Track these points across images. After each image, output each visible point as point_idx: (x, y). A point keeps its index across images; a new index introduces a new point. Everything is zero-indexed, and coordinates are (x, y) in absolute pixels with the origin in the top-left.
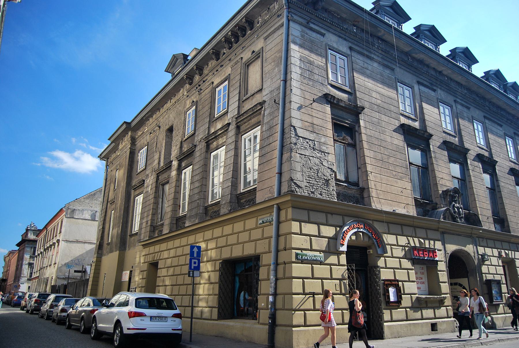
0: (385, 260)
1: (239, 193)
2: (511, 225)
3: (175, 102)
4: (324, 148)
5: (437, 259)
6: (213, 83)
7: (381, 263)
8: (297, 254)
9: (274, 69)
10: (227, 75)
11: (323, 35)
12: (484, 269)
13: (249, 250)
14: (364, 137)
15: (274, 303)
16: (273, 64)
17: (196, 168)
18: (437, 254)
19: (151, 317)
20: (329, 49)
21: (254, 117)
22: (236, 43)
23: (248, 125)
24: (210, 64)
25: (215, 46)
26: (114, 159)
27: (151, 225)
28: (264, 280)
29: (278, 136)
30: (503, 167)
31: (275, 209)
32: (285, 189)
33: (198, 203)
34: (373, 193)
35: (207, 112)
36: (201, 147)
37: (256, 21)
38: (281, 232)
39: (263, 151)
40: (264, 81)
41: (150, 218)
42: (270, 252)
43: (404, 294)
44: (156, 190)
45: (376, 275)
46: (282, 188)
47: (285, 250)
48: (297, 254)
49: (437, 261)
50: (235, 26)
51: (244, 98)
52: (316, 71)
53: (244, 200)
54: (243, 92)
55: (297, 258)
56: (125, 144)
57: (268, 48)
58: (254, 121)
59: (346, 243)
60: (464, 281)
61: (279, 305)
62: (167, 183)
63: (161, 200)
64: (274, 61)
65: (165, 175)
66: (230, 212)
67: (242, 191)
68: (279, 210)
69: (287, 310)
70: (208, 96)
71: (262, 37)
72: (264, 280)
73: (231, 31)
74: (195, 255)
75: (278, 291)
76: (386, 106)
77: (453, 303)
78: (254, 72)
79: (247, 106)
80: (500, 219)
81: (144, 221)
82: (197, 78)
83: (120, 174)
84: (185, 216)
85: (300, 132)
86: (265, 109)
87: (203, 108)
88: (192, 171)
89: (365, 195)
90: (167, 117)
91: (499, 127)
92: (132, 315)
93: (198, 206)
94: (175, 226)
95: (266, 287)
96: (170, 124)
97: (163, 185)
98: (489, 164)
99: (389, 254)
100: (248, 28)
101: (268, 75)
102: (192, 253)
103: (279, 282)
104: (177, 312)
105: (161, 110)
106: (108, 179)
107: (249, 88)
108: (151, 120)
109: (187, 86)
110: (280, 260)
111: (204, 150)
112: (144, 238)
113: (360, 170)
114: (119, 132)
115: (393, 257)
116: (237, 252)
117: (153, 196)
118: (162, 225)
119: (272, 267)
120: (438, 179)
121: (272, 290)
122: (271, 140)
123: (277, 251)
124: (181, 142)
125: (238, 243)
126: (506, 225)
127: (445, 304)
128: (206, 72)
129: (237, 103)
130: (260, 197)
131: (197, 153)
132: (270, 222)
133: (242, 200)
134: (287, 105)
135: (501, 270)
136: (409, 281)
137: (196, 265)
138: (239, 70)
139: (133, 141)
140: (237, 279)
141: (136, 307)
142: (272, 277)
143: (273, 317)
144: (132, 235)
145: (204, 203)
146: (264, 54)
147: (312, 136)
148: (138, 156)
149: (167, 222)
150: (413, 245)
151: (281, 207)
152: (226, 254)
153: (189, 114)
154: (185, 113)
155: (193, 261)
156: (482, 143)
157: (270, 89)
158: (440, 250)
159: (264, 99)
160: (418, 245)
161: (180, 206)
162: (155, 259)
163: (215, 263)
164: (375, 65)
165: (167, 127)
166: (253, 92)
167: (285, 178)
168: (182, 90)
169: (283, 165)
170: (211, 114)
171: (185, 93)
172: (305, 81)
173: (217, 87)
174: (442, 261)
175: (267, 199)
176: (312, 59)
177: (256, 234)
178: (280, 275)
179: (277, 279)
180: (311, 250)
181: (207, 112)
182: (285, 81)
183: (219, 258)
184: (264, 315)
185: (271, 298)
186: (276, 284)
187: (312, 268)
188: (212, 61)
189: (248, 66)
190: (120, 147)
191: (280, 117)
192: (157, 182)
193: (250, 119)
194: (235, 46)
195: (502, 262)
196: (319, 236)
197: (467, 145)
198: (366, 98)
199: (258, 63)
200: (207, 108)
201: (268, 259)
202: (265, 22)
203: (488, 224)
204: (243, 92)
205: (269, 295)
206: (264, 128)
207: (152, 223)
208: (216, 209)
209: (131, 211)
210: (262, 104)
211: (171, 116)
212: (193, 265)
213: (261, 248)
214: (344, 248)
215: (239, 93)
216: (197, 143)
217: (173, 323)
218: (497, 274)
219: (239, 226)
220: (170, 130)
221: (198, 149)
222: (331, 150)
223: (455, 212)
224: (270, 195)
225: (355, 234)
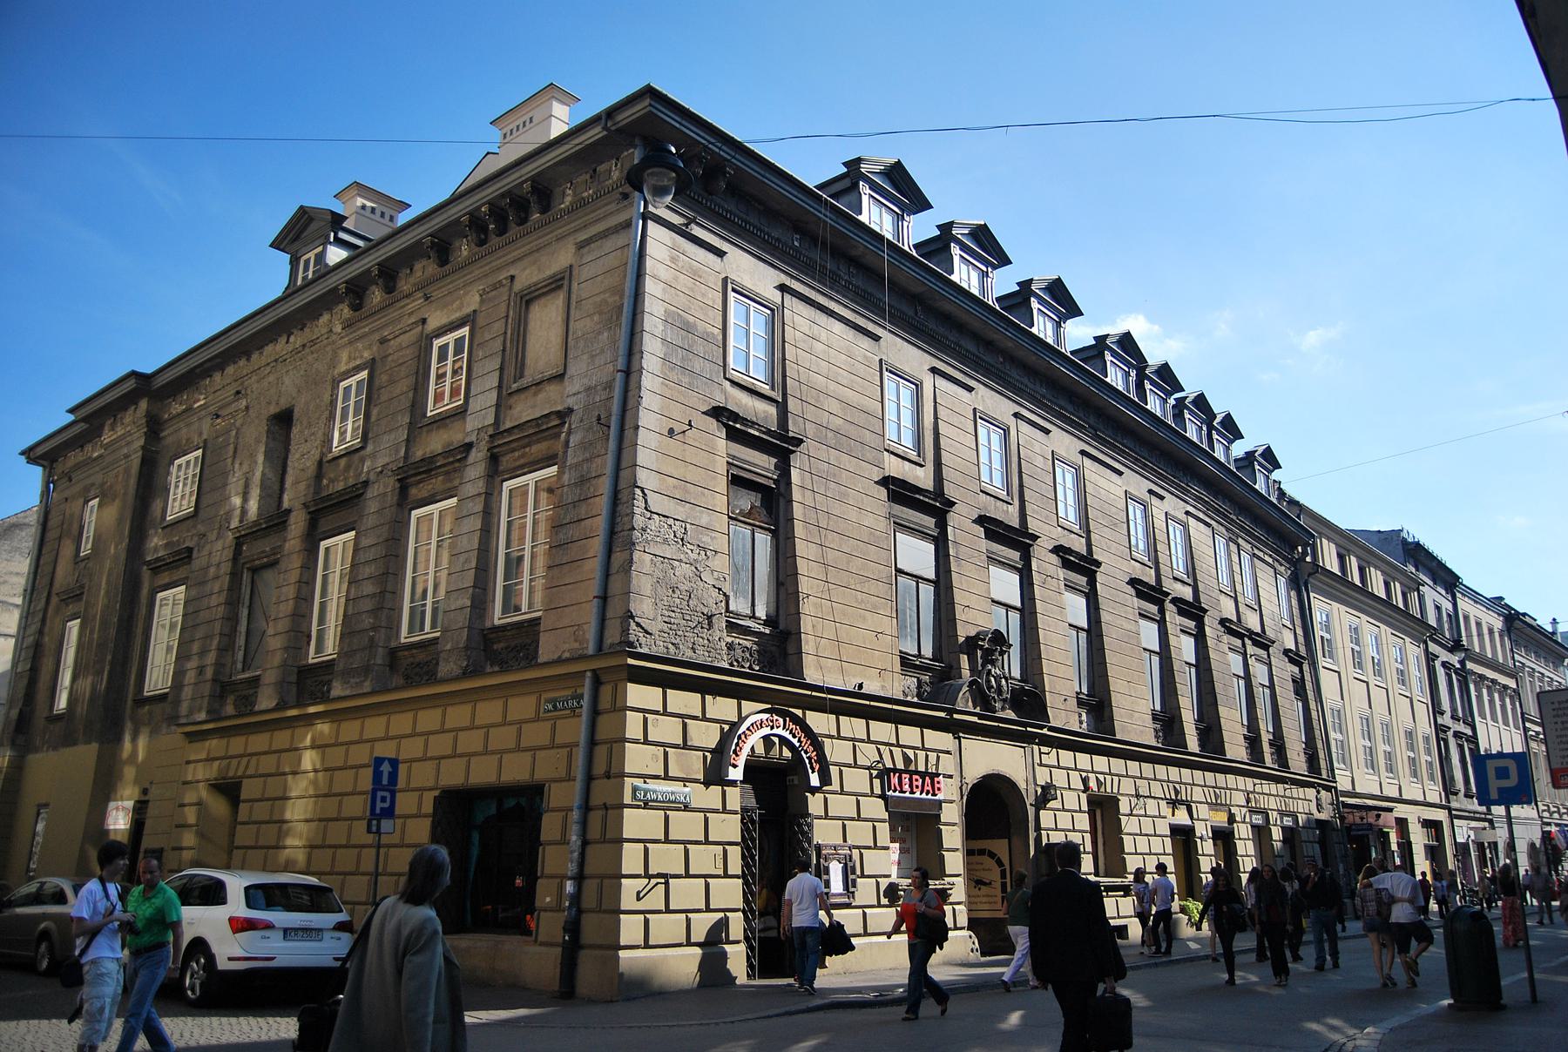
0: (826, 799)
1: (488, 624)
2: (1117, 714)
3: (304, 346)
4: (706, 539)
5: (940, 796)
6: (424, 321)
7: (815, 804)
8: (635, 789)
9: (599, 333)
10: (468, 310)
11: (720, 254)
12: (1046, 818)
13: (516, 771)
14: (797, 511)
15: (576, 898)
16: (596, 318)
17: (365, 542)
18: (942, 786)
19: (286, 930)
20: (734, 290)
21: (538, 441)
22: (500, 235)
23: (523, 456)
24: (418, 266)
25: (440, 230)
26: (78, 466)
27: (214, 680)
28: (550, 843)
29: (602, 504)
30: (1114, 573)
31: (588, 682)
32: (612, 636)
33: (372, 639)
34: (808, 645)
35: (397, 388)
36: (381, 492)
37: (558, 190)
38: (599, 736)
39: (561, 536)
40: (571, 355)
41: (211, 658)
42: (570, 778)
43: (863, 876)
44: (232, 581)
45: (804, 834)
46: (607, 633)
47: (608, 777)
48: (635, 789)
49: (940, 802)
50: (503, 196)
51: (515, 386)
52: (700, 348)
53: (502, 645)
54: (510, 371)
55: (634, 797)
56: (127, 433)
57: (586, 273)
58: (537, 449)
59: (741, 762)
60: (1000, 847)
61: (589, 900)
62: (273, 564)
63: (245, 612)
64: (600, 313)
65: (265, 545)
66: (466, 674)
67: (497, 622)
68: (597, 683)
69: (605, 912)
70: (409, 353)
71: (571, 239)
72: (550, 843)
73: (489, 202)
74: (385, 781)
75: (588, 870)
76: (852, 431)
77: (969, 896)
78: (545, 322)
79: (524, 411)
80: (1098, 703)
81: (192, 664)
82: (376, 296)
83: (96, 518)
84: (329, 665)
85: (656, 502)
86: (570, 428)
87: (392, 382)
88: (356, 550)
89: (791, 649)
90: (277, 378)
91: (1114, 476)
92: (240, 925)
93: (372, 644)
94: (294, 689)
95: (557, 860)
96: (284, 403)
97: (255, 571)
98: (1082, 565)
99: (835, 786)
100: (534, 206)
101: (581, 344)
102: (377, 775)
103: (589, 849)
104: (342, 917)
105: (255, 356)
106: (50, 524)
107: (528, 361)
108: (217, 377)
109: (345, 311)
110: (596, 800)
111: (391, 499)
112: (191, 712)
113: (782, 590)
114: (109, 397)
115: (842, 792)
116: (483, 774)
117: (222, 599)
118: (255, 682)
119: (575, 815)
120: (958, 609)
121: (572, 868)
122: (583, 510)
123: (589, 778)
124: (320, 463)
125: (486, 752)
126: (1106, 714)
127: (951, 899)
128: (404, 285)
129: (494, 394)
130: (548, 648)
131: (370, 503)
132: (573, 710)
133: (502, 649)
134: (628, 433)
135: (1083, 821)
136: (876, 847)
137: (386, 805)
138: (503, 307)
139: (154, 427)
140: (476, 837)
141: (249, 905)
142: (574, 838)
143: (573, 927)
144: (141, 701)
145: (389, 639)
146: (575, 285)
147: (679, 511)
148: (168, 473)
149: (270, 677)
150: (889, 765)
151: (604, 678)
152: (453, 776)
153: (348, 389)
154: (335, 384)
155: (380, 794)
156: (1072, 517)
157: (586, 381)
158: (951, 777)
159: (570, 402)
160: (900, 765)
161: (309, 637)
162: (231, 774)
163: (421, 797)
164: (838, 327)
165: (273, 410)
166: (538, 377)
167: (614, 611)
168: (325, 318)
169: (612, 579)
170: (417, 405)
171: (338, 328)
172: (673, 376)
173: (438, 336)
174: (951, 802)
175: (567, 655)
176: (691, 319)
177: (537, 734)
178: (594, 832)
179: (585, 843)
180: (667, 777)
181: (397, 388)
182: (627, 373)
183: (431, 784)
184: (550, 925)
185: (569, 887)
186: (583, 855)
187: (667, 818)
188: (424, 262)
189: (528, 303)
190: (107, 437)
191: (610, 459)
192: (235, 559)
193: (529, 445)
194: (495, 241)
195: (1089, 802)
196: (685, 746)
197: (1033, 526)
198: (810, 412)
199: (559, 300)
200: (404, 385)
201: (563, 796)
202: (581, 204)
203: (1065, 714)
204: (510, 371)
205: (564, 877)
206: (566, 477)
207: (216, 673)
208: (421, 656)
209: (139, 631)
210: (564, 415)
211: (287, 381)
212: (379, 805)
213: (547, 767)
214: (736, 774)
215: (502, 369)
216: (372, 477)
217: (334, 943)
218: (1074, 830)
219: (489, 711)
220: (283, 420)
221: (372, 492)
222: (721, 543)
223: (990, 687)
224: (576, 645)
225: (766, 738)
